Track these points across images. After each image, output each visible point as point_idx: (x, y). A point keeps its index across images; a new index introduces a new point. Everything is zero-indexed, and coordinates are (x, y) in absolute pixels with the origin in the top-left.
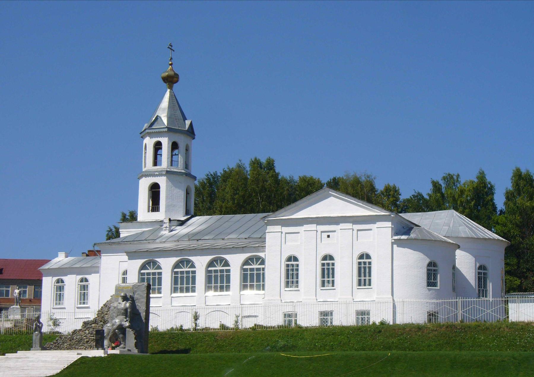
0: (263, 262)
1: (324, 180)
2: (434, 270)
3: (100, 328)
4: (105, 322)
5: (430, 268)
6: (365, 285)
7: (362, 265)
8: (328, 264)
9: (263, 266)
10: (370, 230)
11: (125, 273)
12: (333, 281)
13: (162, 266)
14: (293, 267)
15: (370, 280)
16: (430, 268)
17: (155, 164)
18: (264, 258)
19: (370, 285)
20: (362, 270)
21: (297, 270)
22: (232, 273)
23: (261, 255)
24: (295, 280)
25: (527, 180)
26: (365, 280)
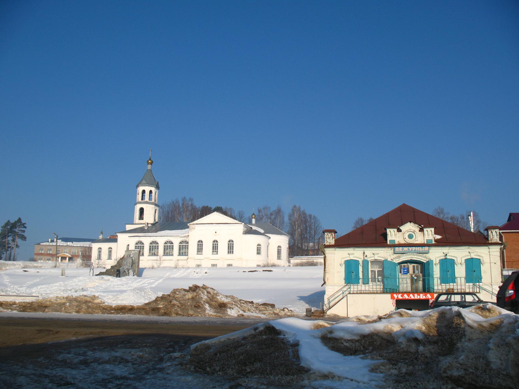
0: (188, 243)
1: (213, 207)
2: (260, 248)
3: (118, 269)
4: (121, 267)
5: (278, 248)
6: (231, 253)
7: (214, 245)
8: (215, 244)
9: (188, 244)
10: (271, 271)
11: (128, 245)
12: (217, 251)
13: (144, 243)
14: (200, 245)
15: (233, 251)
16: (278, 248)
17: (142, 199)
18: (517, 274)
19: (233, 253)
20: (232, 246)
21: (202, 246)
22: (159, 248)
23: (187, 240)
24: (216, 250)
25: (158, 309)
26: (231, 251)
